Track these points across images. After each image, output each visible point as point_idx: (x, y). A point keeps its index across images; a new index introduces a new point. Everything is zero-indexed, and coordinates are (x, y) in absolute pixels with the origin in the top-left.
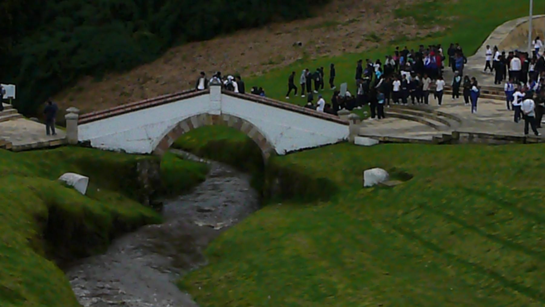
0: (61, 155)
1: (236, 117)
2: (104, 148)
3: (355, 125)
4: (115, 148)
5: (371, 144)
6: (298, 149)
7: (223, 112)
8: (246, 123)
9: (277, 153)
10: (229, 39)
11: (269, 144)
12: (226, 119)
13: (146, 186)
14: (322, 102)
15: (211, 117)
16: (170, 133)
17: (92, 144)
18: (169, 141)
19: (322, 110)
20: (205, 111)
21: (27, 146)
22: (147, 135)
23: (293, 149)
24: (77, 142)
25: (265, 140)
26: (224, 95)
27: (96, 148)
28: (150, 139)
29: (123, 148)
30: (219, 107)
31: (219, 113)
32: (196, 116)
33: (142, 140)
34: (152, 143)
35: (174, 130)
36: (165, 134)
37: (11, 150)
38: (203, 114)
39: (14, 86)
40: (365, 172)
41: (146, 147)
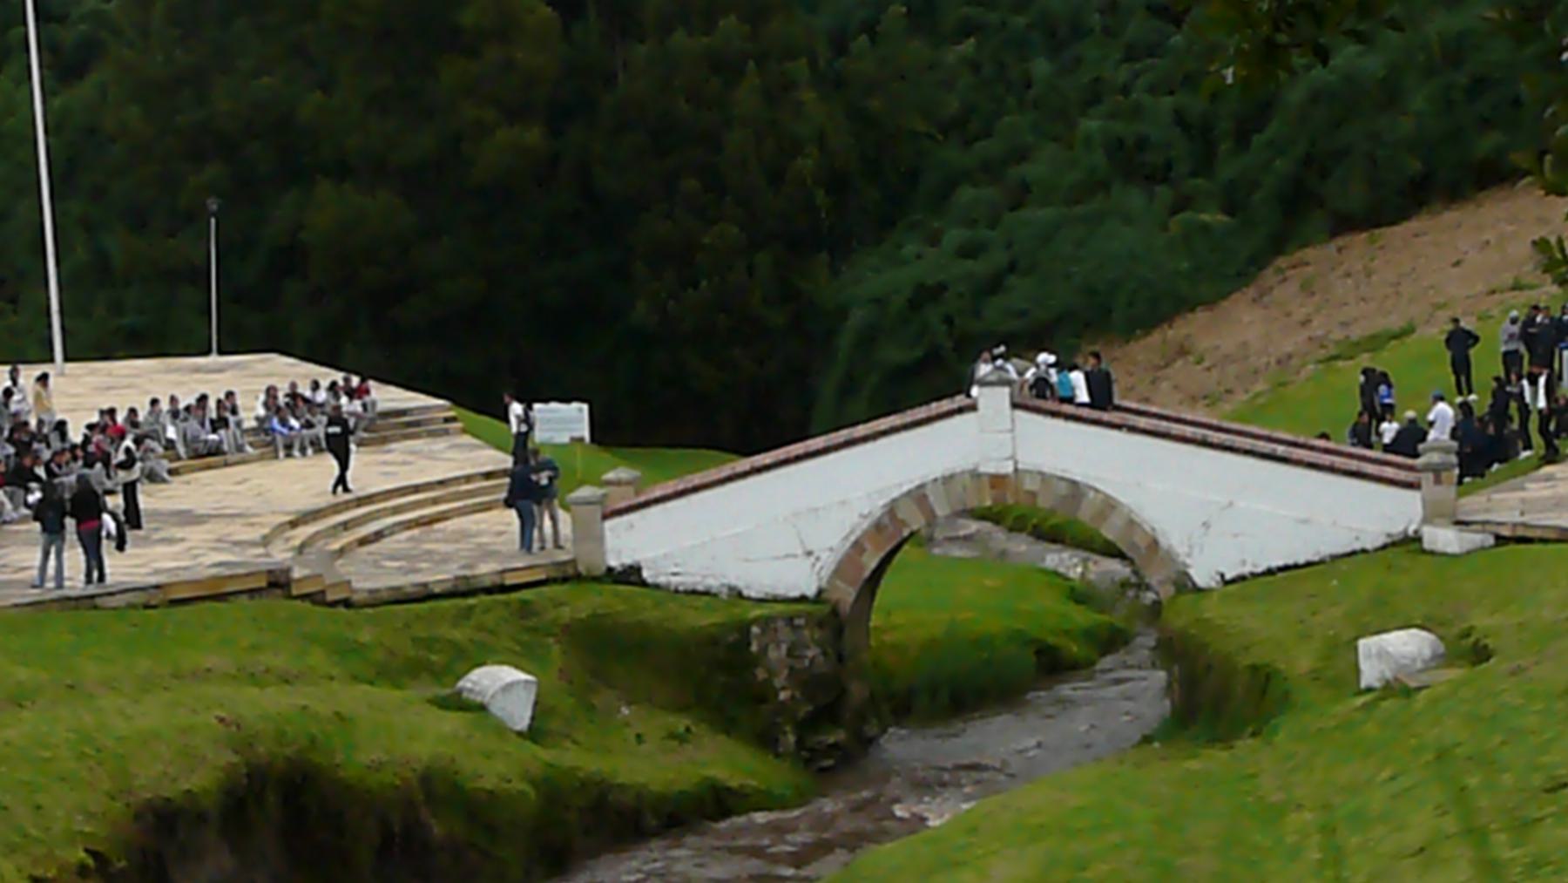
0: (525, 610)
1: (1062, 479)
2: (682, 584)
3: (1438, 488)
4: (713, 583)
5: (1467, 546)
6: (1259, 570)
7: (1020, 466)
8: (1092, 494)
9: (1194, 584)
10: (1451, 216)
11: (1170, 557)
12: (1030, 485)
13: (783, 696)
14: (1443, 415)
15: (986, 481)
16: (865, 533)
17: (645, 574)
18: (865, 558)
19: (1446, 436)
21: (410, 590)
22: (802, 542)
23: (1246, 570)
24: (604, 569)
25: (1154, 544)
26: (1020, 414)
27: (657, 587)
28: (809, 553)
29: (733, 582)
30: (1008, 453)
31: (1008, 468)
32: (940, 482)
33: (787, 556)
34: (818, 565)
35: (878, 527)
36: (853, 538)
37: (347, 603)
38: (963, 473)
39: (585, 407)
40: (1363, 643)
41: (801, 579)
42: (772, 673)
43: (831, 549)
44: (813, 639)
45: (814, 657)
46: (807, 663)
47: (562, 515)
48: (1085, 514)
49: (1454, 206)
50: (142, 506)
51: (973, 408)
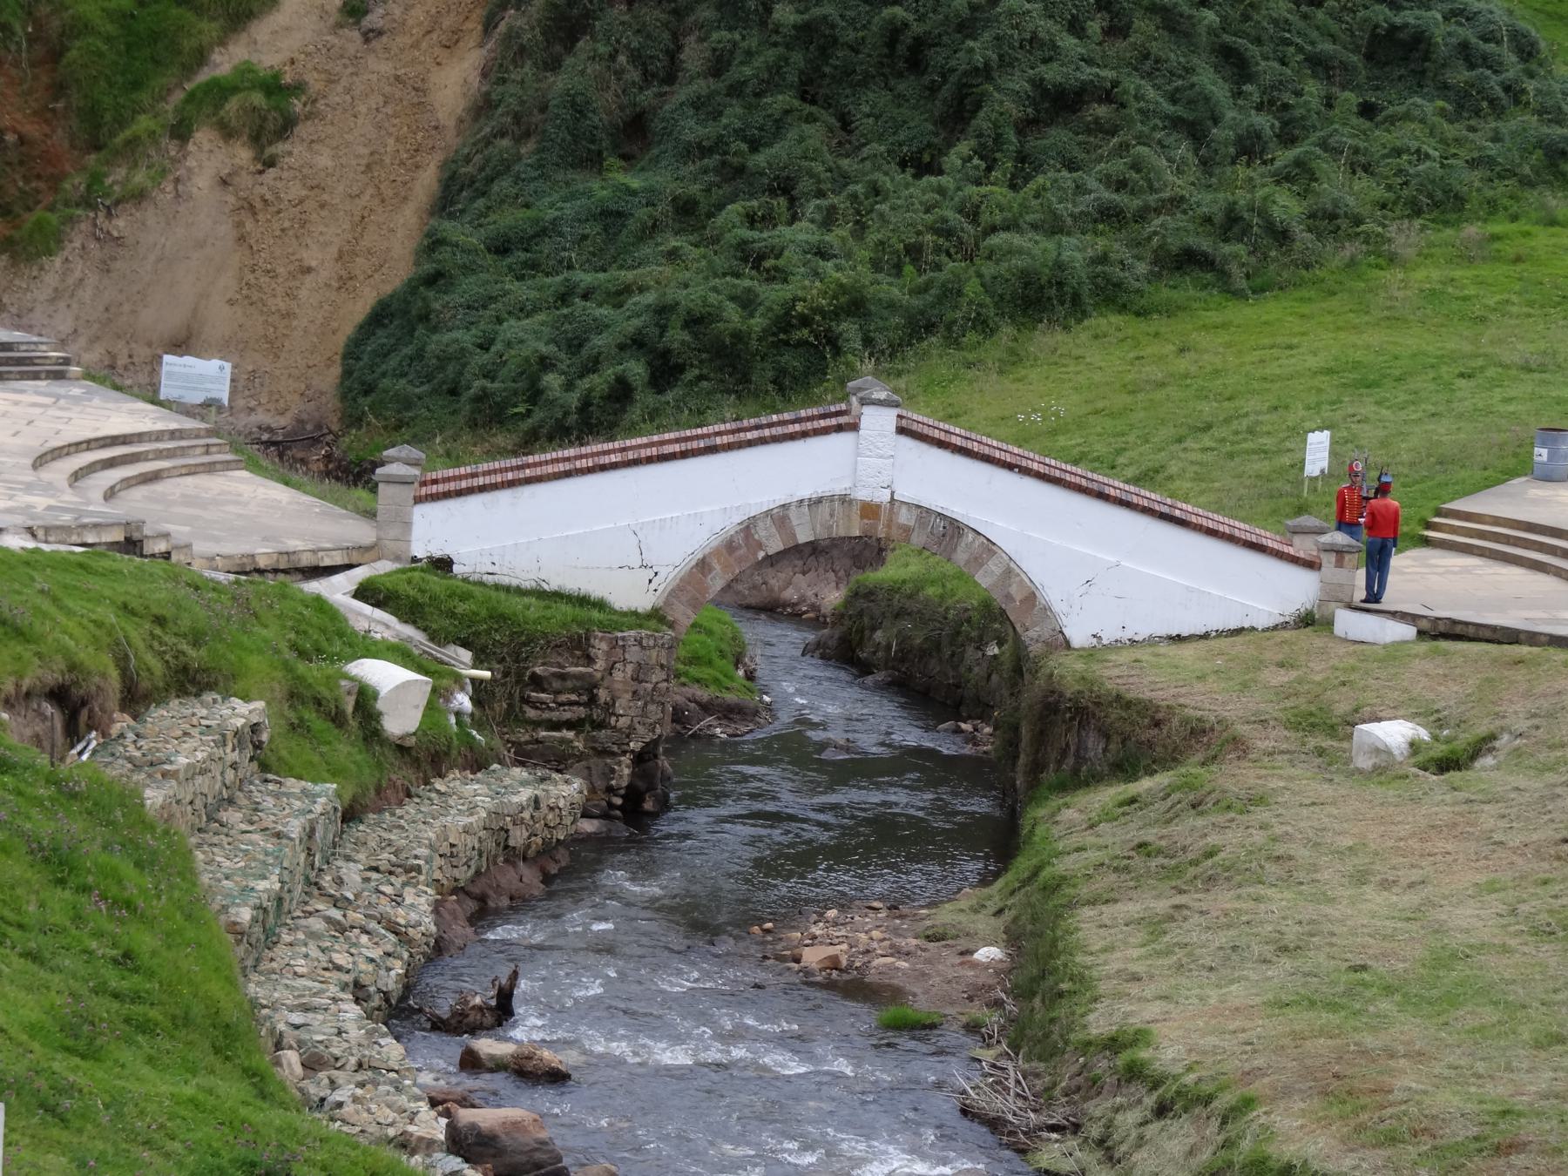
16: (716, 552)
20: (838, 488)
31: (885, 496)
35: (730, 546)
39: (228, 366)
46: (649, 686)
50: (781, 547)
51: (854, 427)
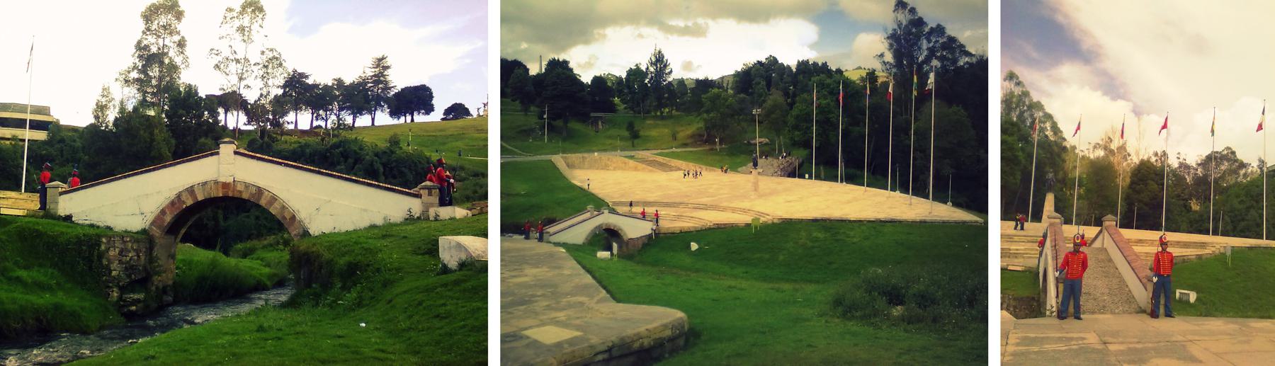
4: (100, 224)
12: (239, 187)
16: (167, 207)
17: (73, 219)
25: (293, 217)
28: (142, 214)
35: (172, 203)
42: (110, 262)
43: (152, 212)
44: (132, 247)
45: (132, 257)
47: (1058, 221)
48: (263, 202)
49: (1060, 18)
